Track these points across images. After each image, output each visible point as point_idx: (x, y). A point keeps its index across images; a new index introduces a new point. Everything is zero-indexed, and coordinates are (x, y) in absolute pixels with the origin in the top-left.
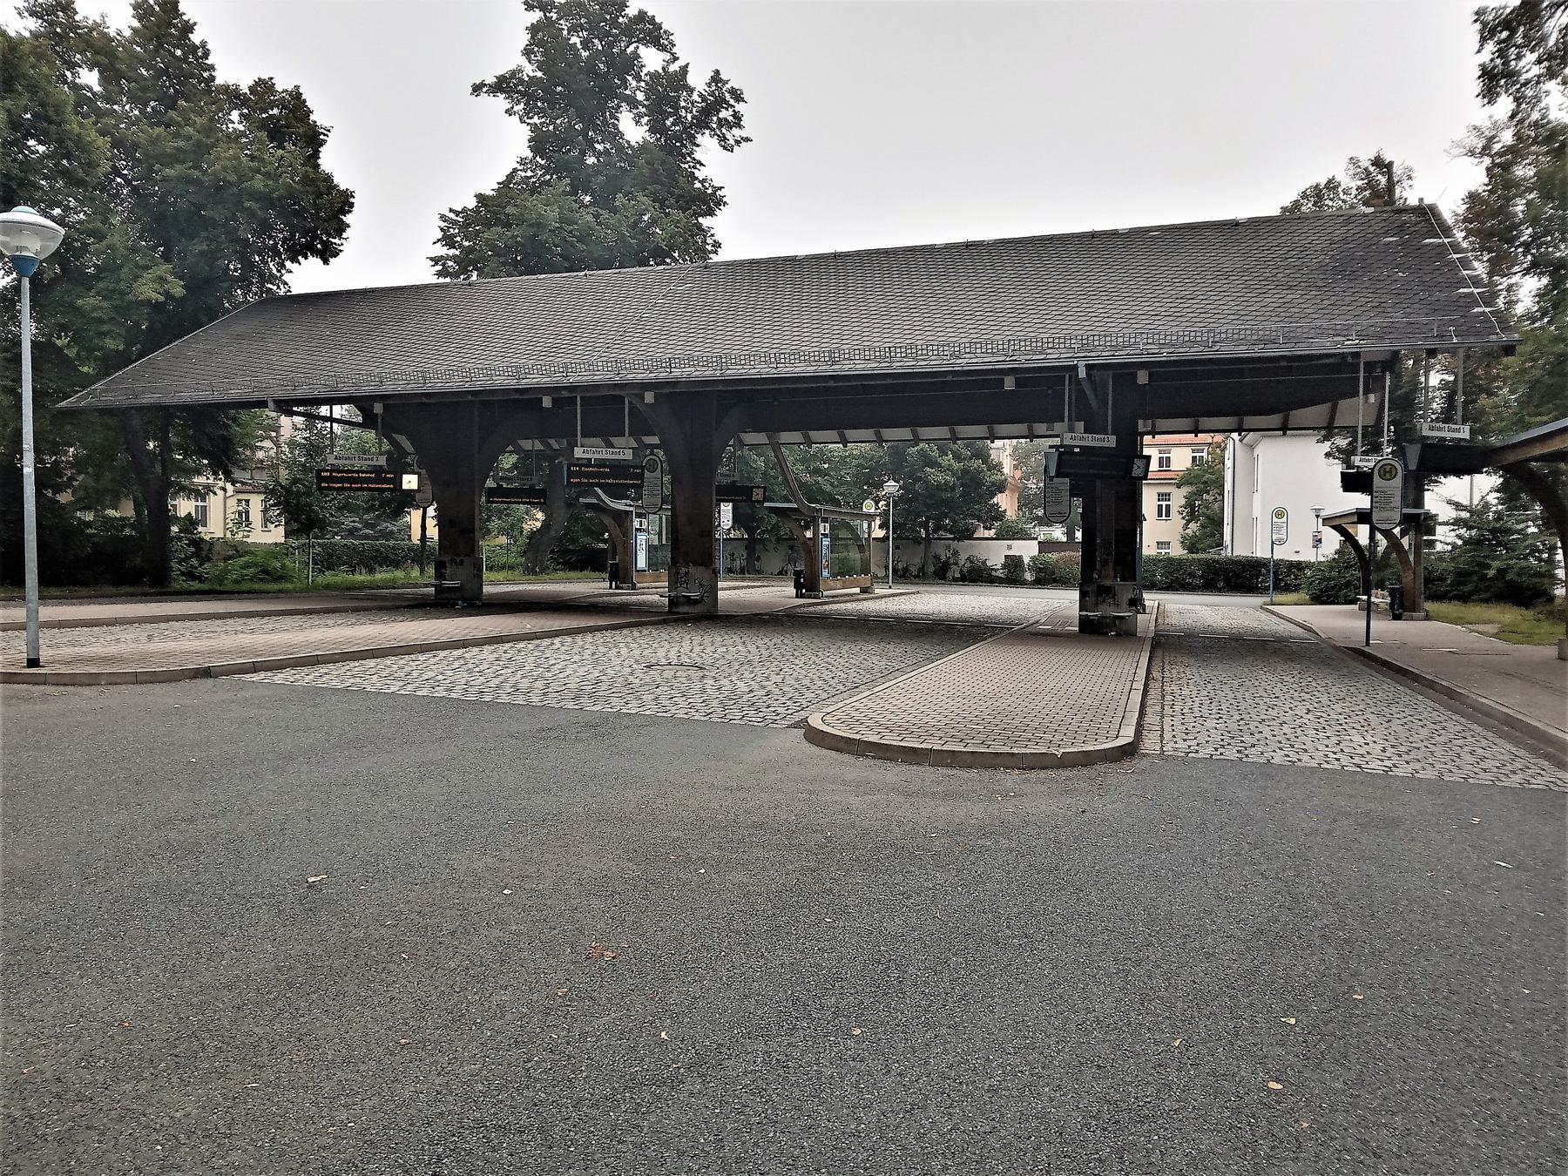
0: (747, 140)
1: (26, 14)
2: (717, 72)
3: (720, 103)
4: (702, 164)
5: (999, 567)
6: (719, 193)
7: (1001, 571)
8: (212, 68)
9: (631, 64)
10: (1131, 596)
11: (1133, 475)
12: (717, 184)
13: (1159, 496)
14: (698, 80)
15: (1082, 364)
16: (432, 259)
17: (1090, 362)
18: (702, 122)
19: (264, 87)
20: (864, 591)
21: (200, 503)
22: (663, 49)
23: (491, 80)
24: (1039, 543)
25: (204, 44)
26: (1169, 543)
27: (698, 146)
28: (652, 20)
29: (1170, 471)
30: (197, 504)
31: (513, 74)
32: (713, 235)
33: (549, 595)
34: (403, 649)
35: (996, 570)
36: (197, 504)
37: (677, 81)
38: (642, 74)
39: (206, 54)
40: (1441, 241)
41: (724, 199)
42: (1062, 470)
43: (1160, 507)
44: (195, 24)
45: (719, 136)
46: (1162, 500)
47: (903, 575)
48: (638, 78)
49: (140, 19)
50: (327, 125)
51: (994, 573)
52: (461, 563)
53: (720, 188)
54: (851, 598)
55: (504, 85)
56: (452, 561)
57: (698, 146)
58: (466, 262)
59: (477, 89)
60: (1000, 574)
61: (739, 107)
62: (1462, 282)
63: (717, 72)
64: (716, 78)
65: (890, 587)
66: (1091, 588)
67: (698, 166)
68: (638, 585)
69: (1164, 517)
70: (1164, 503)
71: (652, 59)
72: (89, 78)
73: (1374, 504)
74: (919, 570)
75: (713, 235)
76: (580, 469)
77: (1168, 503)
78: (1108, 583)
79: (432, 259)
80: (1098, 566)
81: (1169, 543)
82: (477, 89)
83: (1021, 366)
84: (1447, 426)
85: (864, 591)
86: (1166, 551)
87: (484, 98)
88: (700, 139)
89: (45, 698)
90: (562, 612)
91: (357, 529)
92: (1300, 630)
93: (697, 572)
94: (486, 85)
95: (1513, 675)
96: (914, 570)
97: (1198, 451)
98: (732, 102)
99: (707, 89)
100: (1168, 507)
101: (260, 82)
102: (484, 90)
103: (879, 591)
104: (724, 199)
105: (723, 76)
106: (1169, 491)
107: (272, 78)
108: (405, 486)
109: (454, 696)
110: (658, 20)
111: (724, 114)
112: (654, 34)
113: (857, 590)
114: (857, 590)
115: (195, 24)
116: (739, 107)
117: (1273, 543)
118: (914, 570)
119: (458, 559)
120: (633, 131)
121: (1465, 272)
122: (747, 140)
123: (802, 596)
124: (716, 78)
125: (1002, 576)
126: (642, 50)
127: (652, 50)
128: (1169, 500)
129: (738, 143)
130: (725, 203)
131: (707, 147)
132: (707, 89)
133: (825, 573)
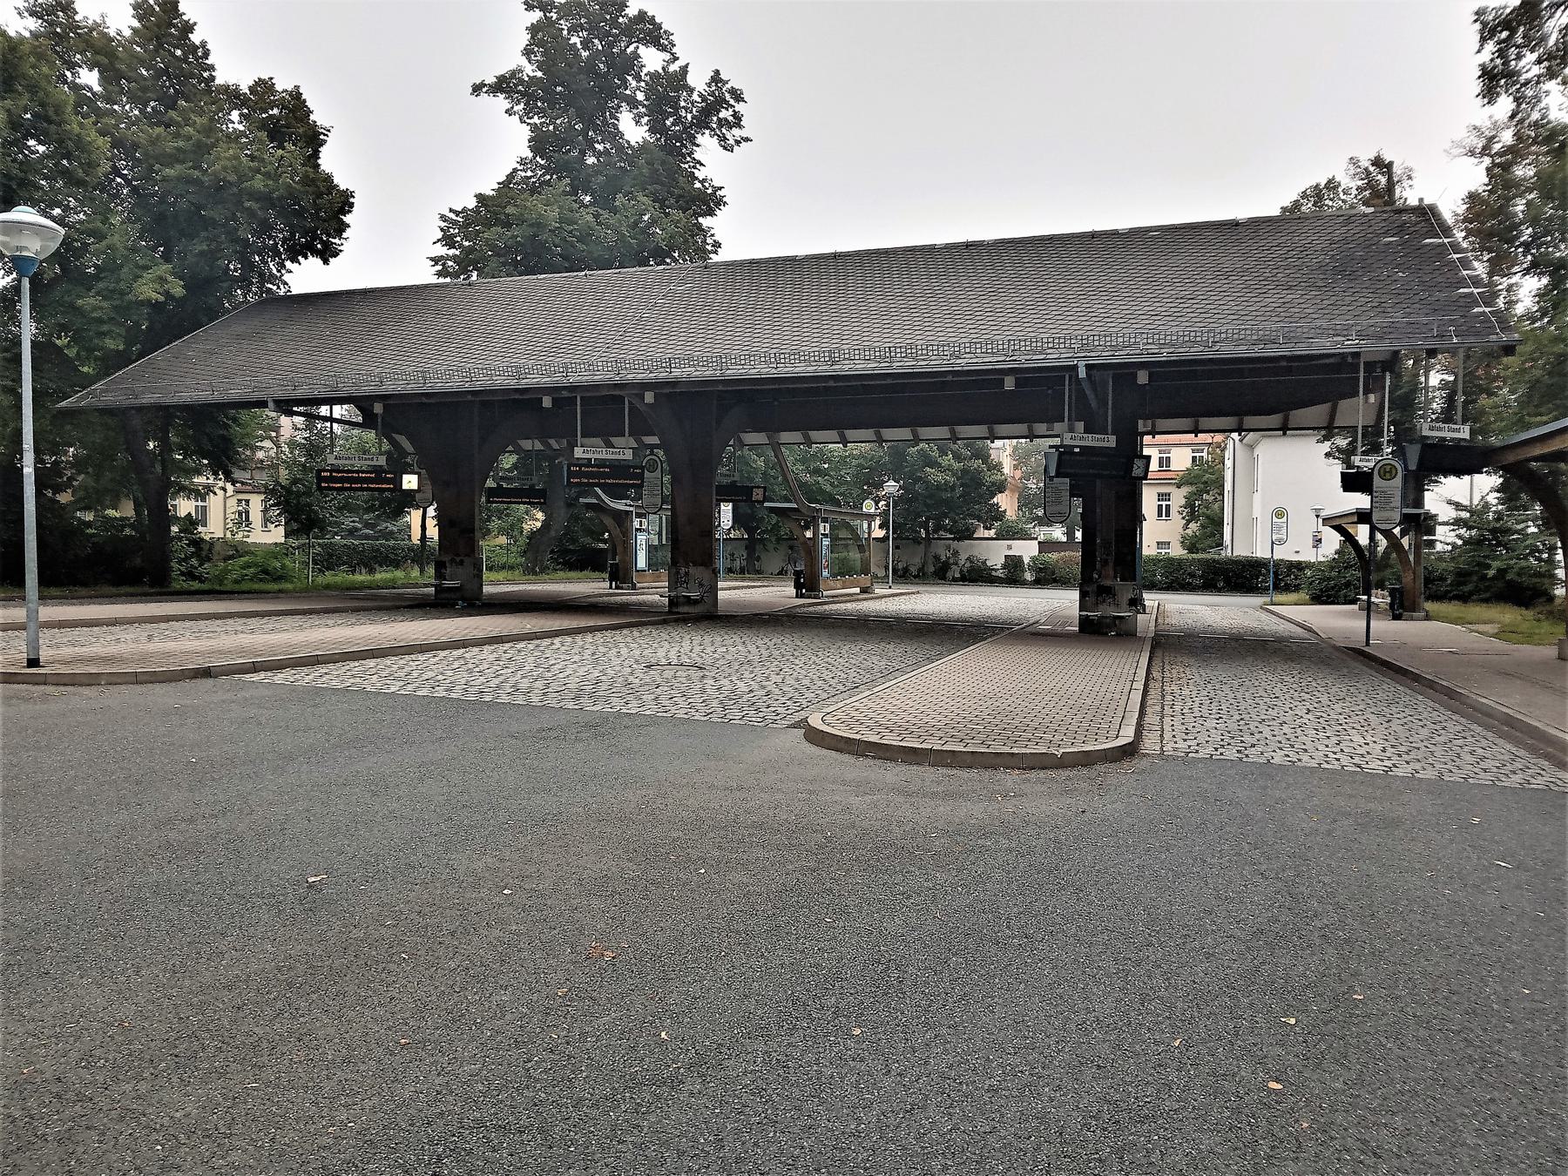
0: (747, 140)
1: (26, 14)
2: (717, 72)
3: (720, 103)
4: (702, 164)
5: (999, 567)
6: (719, 193)
7: (1001, 571)
8: (212, 68)
9: (631, 64)
10: (1131, 596)
11: (1133, 475)
12: (717, 184)
13: (1159, 496)
14: (698, 80)
15: (1082, 364)
16: (432, 259)
17: (1090, 362)
18: (702, 122)
19: (264, 87)
20: (864, 591)
21: (200, 503)
22: (663, 49)
23: (491, 80)
24: (1039, 543)
25: (204, 44)
26: (1169, 543)
27: (698, 146)
28: (652, 20)
29: (1170, 471)
30: (197, 504)
31: (513, 74)
32: (713, 235)
33: (549, 595)
35: (996, 570)
36: (197, 504)
37: (677, 81)
38: (642, 74)
39: (206, 54)
40: (1441, 241)
41: (724, 199)
42: (1062, 470)
43: (1160, 507)
44: (195, 24)
45: (719, 136)
46: (1162, 500)
47: (903, 575)
48: (638, 78)
49: (140, 19)
50: (327, 125)
51: (994, 573)
52: (461, 563)
53: (720, 188)
54: (851, 598)
55: (504, 85)
56: (452, 561)
57: (698, 146)
58: (466, 262)
59: (477, 89)
60: (1000, 574)
61: (739, 107)
62: (1462, 282)
63: (717, 72)
64: (716, 78)
65: (890, 587)
66: (1091, 588)
67: (698, 166)
68: (638, 585)
69: (1164, 517)
70: (1164, 503)
71: (652, 59)
72: (89, 78)
73: (1374, 504)
74: (919, 570)
75: (713, 235)
76: (580, 469)
77: (1168, 503)
78: (1108, 583)
79: (432, 259)
80: (1098, 566)
81: (1169, 543)
82: (477, 89)
83: (1021, 366)
84: (1447, 426)
85: (864, 591)
86: (1166, 551)
87: (484, 98)
88: (700, 139)
89: (45, 698)
90: (562, 612)
91: (357, 529)
92: (1300, 630)
93: (697, 572)
94: (486, 85)
95: (1513, 675)
96: (914, 570)
97: (1198, 451)
98: (732, 102)
99: (707, 89)
100: (1168, 507)
101: (260, 82)
102: (484, 90)
103: (879, 591)
104: (724, 199)
105: (723, 76)
106: (1169, 491)
107: (272, 78)
108: (405, 486)
109: (454, 696)
110: (658, 20)
111: (724, 114)
112: (654, 34)
113: (857, 590)
114: (857, 590)
115: (195, 24)
116: (739, 107)
117: (1273, 543)
118: (914, 570)
119: (458, 559)
120: (633, 131)
121: (1465, 272)
122: (747, 140)
123: (802, 596)
124: (716, 78)
125: (1002, 576)
126: (642, 50)
127: (652, 50)
128: (1169, 500)
129: (738, 143)
130: (725, 203)
131: (707, 147)
132: (707, 89)
133: (825, 573)
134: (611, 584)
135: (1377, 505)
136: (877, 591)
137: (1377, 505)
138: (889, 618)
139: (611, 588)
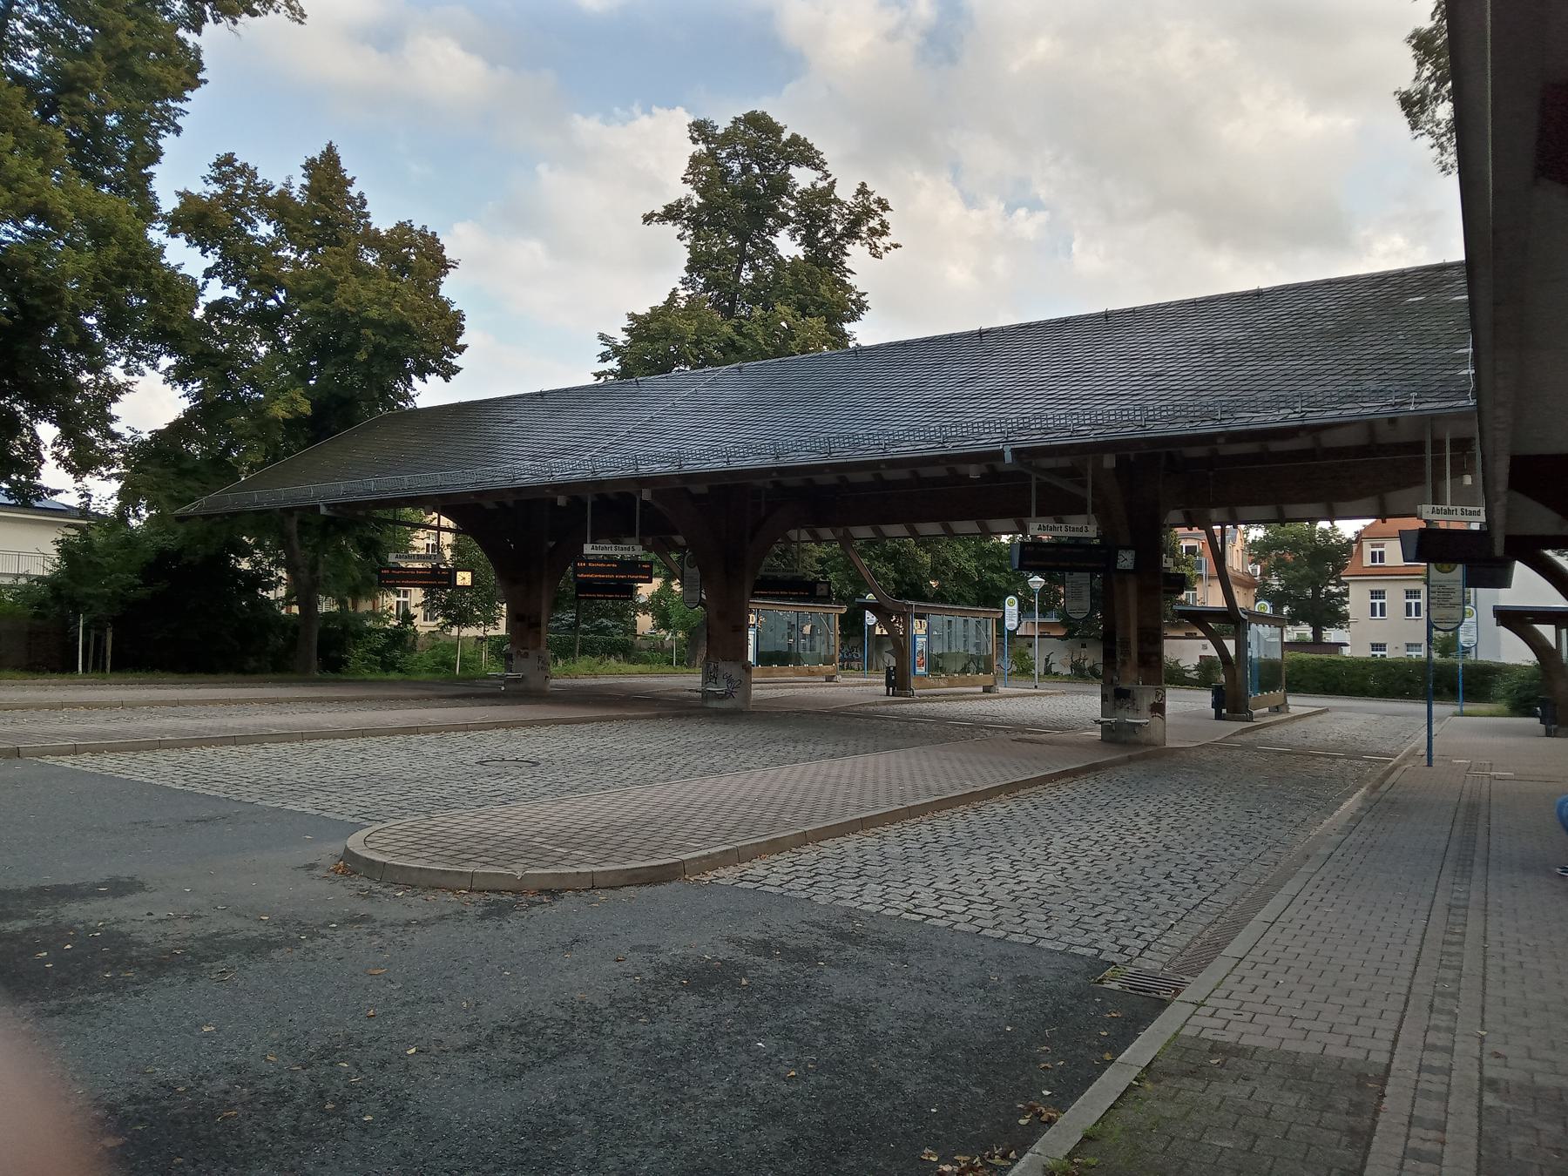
0: (896, 246)
1: (211, 181)
2: (863, 185)
3: (868, 213)
4: (853, 273)
5: (1192, 668)
6: (863, 298)
7: (1195, 673)
8: (367, 215)
9: (781, 186)
10: (1153, 700)
11: (1118, 567)
12: (860, 290)
13: (1407, 592)
14: (845, 192)
15: (1007, 449)
16: (595, 375)
17: (1016, 446)
18: (851, 233)
19: (403, 228)
20: (987, 690)
21: (401, 599)
22: (817, 168)
23: (660, 210)
25: (361, 195)
26: (1385, 645)
27: (848, 255)
29: (1384, 567)
30: (398, 599)
31: (679, 204)
32: (855, 339)
33: (619, 688)
34: (274, 737)
35: (1189, 671)
36: (398, 599)
37: (825, 196)
38: (795, 193)
39: (364, 203)
41: (867, 304)
42: (1026, 563)
45: (870, 244)
46: (1411, 597)
48: (792, 197)
49: (309, 177)
50: (454, 258)
51: (1187, 675)
52: (526, 655)
53: (864, 294)
54: (973, 698)
55: (672, 213)
56: (518, 652)
57: (848, 255)
58: (625, 373)
59: (648, 219)
60: (1194, 675)
61: (886, 216)
63: (863, 185)
64: (863, 191)
66: (1111, 691)
67: (848, 274)
70: (1378, 602)
71: (802, 177)
72: (265, 229)
73: (1431, 601)
75: (855, 339)
76: (587, 565)
78: (1126, 686)
79: (595, 375)
81: (1385, 645)
82: (648, 219)
83: (948, 452)
84: (1459, 508)
85: (987, 690)
86: (1383, 653)
87: (656, 227)
88: (849, 249)
93: (726, 668)
94: (655, 215)
97: (1378, 546)
98: (880, 211)
99: (854, 201)
100: (1382, 605)
101: (400, 225)
102: (655, 219)
103: (1002, 690)
104: (867, 304)
105: (869, 189)
106: (1380, 588)
107: (410, 221)
108: (459, 582)
110: (810, 142)
111: (874, 223)
112: (804, 154)
113: (981, 689)
116: (886, 216)
119: (523, 651)
120: (788, 246)
122: (896, 246)
124: (863, 191)
125: (1197, 677)
126: (793, 170)
127: (805, 169)
128: (1384, 598)
129: (887, 249)
130: (868, 308)
131: (856, 255)
132: (854, 201)
133: (921, 670)
134: (888, 690)
135: (1435, 595)
136: (1292, 709)
137: (1435, 595)
138: (1006, 724)
139: (888, 694)
